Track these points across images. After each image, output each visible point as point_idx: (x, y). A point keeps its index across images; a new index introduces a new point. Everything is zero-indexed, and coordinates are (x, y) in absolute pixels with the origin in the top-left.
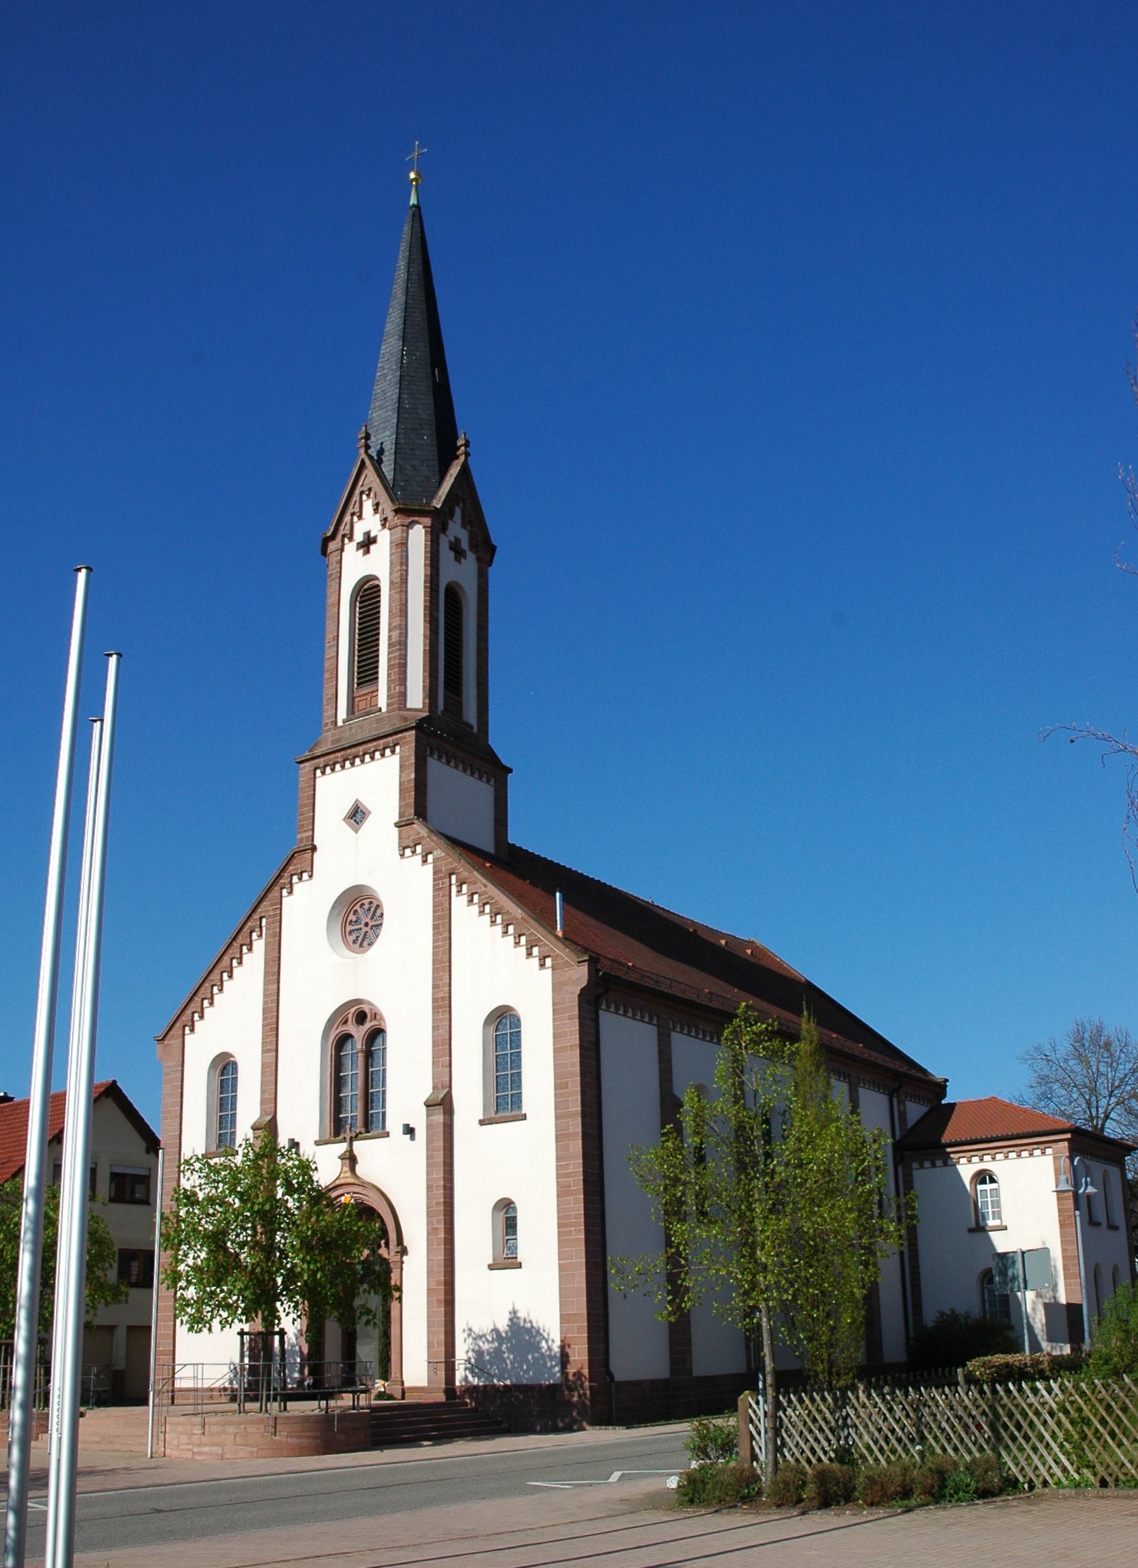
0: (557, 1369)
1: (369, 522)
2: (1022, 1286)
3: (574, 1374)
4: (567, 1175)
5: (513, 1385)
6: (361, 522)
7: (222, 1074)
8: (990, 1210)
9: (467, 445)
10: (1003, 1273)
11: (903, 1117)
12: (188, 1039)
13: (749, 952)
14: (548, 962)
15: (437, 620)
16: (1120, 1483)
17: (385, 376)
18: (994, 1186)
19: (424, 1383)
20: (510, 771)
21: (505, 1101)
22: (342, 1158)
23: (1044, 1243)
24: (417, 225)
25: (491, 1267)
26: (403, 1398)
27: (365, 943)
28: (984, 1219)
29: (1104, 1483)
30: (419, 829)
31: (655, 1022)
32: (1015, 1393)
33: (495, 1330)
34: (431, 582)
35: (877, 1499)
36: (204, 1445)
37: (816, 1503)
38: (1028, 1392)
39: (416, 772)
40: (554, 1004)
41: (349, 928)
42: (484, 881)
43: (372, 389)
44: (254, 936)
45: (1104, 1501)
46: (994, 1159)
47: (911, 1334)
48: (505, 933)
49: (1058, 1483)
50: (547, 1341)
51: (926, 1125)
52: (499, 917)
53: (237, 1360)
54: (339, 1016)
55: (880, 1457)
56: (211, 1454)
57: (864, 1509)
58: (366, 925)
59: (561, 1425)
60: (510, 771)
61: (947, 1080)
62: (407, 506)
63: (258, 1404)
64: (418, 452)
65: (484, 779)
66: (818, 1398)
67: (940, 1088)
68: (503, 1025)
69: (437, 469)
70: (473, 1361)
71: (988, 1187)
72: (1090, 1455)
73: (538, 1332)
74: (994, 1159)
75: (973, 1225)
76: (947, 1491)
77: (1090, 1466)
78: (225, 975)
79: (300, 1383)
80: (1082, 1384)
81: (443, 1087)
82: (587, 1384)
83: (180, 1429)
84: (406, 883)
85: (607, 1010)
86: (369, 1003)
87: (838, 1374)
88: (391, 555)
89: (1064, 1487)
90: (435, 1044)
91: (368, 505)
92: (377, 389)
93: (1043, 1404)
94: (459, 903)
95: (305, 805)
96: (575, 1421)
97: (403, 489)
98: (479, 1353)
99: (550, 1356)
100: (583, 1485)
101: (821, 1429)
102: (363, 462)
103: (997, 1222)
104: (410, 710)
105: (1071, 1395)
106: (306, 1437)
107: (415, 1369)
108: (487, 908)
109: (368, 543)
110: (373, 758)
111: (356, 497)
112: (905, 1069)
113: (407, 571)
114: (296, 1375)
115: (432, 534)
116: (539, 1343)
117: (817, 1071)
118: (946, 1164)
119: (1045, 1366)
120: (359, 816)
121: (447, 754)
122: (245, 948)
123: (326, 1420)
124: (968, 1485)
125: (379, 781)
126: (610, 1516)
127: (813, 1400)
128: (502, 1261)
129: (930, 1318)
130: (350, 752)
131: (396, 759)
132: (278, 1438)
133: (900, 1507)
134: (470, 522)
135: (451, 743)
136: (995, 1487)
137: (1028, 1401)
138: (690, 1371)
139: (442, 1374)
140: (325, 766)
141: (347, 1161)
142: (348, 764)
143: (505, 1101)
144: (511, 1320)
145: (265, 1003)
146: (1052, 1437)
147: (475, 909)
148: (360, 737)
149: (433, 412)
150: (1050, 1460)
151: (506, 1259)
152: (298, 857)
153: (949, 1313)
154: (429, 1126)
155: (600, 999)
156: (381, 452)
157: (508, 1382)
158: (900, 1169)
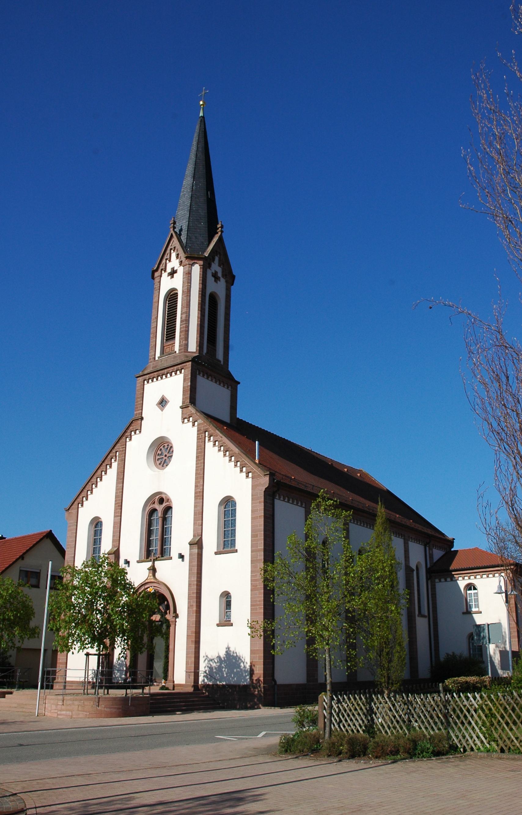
0: (248, 677)
1: (174, 263)
2: (488, 641)
3: (256, 680)
4: (256, 580)
5: (226, 685)
6: (170, 263)
7: (96, 527)
8: (473, 603)
9: (222, 227)
10: (479, 635)
11: (431, 556)
12: (80, 510)
13: (359, 475)
14: (250, 475)
15: (204, 309)
16: (511, 751)
17: (185, 195)
18: (476, 591)
19: (183, 682)
20: (239, 383)
21: (227, 544)
22: (149, 569)
23: (500, 620)
24: (203, 126)
25: (218, 625)
26: (174, 689)
27: (165, 465)
28: (471, 608)
29: (502, 751)
30: (191, 409)
31: (304, 506)
32: (457, 699)
33: (219, 657)
34: (202, 292)
35: (379, 754)
36: (63, 710)
37: (348, 756)
38: (464, 698)
39: (191, 382)
40: (252, 496)
41: (158, 457)
42: (221, 435)
43: (178, 202)
44: (113, 460)
45: (500, 761)
46: (475, 578)
47: (433, 664)
48: (230, 460)
49: (479, 749)
50: (244, 663)
51: (443, 560)
52: (228, 453)
53: (96, 668)
54: (150, 500)
55: (388, 730)
56: (66, 715)
57: (371, 760)
58: (166, 456)
59: (249, 705)
60: (239, 383)
61: (454, 539)
62: (191, 257)
63: (94, 690)
64: (198, 230)
65: (226, 387)
66: (357, 698)
67: (451, 543)
68: (228, 505)
69: (207, 238)
70: (207, 672)
71: (472, 592)
72: (495, 734)
73: (239, 658)
74: (475, 578)
75: (465, 610)
76: (417, 752)
77: (495, 740)
78: (99, 479)
79: (125, 680)
80: (492, 695)
81: (198, 536)
82: (262, 685)
83: (52, 702)
84: (184, 436)
85: (279, 499)
86: (165, 494)
87: (392, 684)
88: (183, 278)
89: (481, 752)
90: (195, 514)
91: (174, 255)
92: (181, 201)
93: (471, 705)
94: (209, 445)
95: (139, 398)
96: (256, 704)
97: (190, 247)
98: (211, 668)
99: (245, 670)
100: (243, 739)
101: (359, 714)
102: (172, 235)
103: (477, 610)
104: (190, 352)
105: (486, 701)
106: (115, 708)
107: (180, 675)
108: (222, 448)
109: (173, 273)
110: (171, 375)
111: (168, 251)
112: (433, 533)
113: (190, 286)
114: (123, 676)
115: (203, 269)
116: (240, 663)
117: (385, 532)
118: (452, 580)
119: (487, 683)
120: (164, 403)
121: (207, 374)
122: (108, 466)
123: (125, 700)
124: (428, 749)
125: (173, 387)
126: (241, 758)
127: (355, 699)
128: (223, 622)
129: (442, 657)
130: (161, 372)
131: (182, 375)
132: (100, 708)
133: (391, 759)
134: (223, 264)
135: (210, 368)
136: (443, 750)
137: (464, 703)
138: (317, 680)
139: (192, 678)
140: (149, 379)
141: (152, 571)
142: (159, 378)
143: (227, 544)
144: (226, 652)
145: (116, 493)
146: (476, 724)
147: (216, 448)
148: (166, 365)
149: (206, 211)
150: (474, 735)
151: (225, 621)
152: (134, 423)
153: (452, 654)
154: (191, 555)
155: (274, 494)
156: (181, 230)
157: (224, 683)
158: (429, 582)
